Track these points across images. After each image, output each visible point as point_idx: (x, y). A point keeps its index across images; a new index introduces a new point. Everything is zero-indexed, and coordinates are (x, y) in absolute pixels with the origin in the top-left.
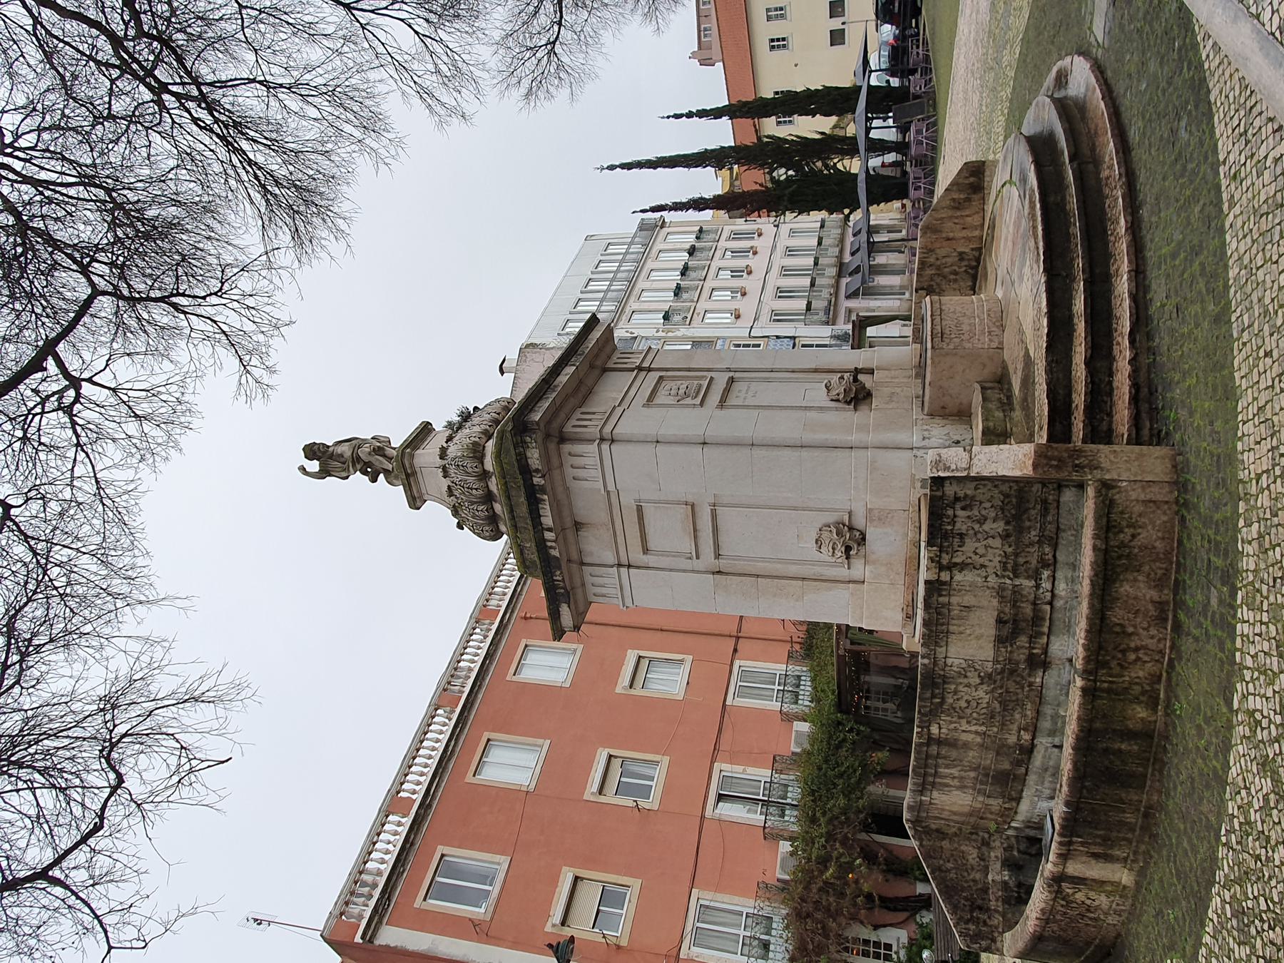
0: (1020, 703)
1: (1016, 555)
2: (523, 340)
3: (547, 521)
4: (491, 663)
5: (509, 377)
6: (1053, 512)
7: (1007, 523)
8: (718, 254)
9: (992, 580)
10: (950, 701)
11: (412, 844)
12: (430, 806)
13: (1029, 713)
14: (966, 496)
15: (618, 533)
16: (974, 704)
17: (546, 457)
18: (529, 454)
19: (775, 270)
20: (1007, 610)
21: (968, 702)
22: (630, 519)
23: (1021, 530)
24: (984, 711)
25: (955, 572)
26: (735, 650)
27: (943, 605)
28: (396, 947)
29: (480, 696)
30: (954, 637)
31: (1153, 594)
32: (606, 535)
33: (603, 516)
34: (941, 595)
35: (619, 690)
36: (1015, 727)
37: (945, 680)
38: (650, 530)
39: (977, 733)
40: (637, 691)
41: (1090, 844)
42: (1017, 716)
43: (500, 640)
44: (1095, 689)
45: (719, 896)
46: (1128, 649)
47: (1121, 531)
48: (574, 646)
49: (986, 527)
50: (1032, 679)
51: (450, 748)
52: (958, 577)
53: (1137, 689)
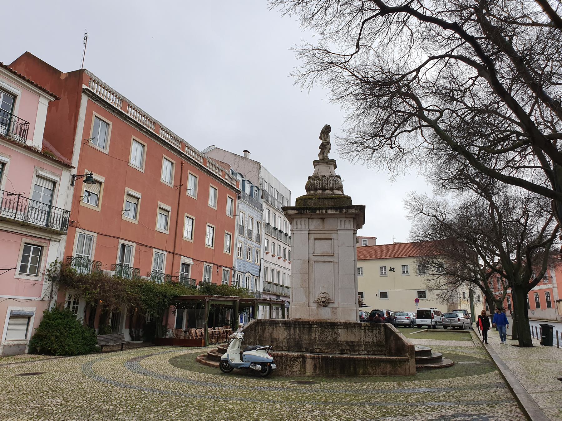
0: (328, 348)
1: (370, 345)
2: (262, 164)
3: (329, 211)
4: (169, 148)
5: (242, 154)
6: (380, 353)
7: (376, 343)
8: (285, 245)
9: (362, 340)
10: (326, 330)
11: (114, 111)
12: (125, 119)
13: (326, 350)
14: (381, 332)
15: (321, 231)
16: (326, 336)
17: (352, 214)
18: (353, 209)
19: (279, 269)
20: (356, 343)
21: (326, 335)
22: (327, 236)
23: (375, 346)
24: (324, 339)
25: (364, 330)
26: (170, 252)
27: (355, 327)
28: (81, 103)
29: (158, 143)
30: (346, 330)
31: (388, 372)
32: (320, 227)
33: (327, 227)
34: (358, 327)
35: (127, 188)
36: (320, 347)
37: (333, 329)
38: (322, 241)
39: (315, 337)
40: (158, 210)
41: (319, 364)
42: (324, 348)
43: (176, 152)
44: (365, 361)
45: (95, 245)
46: (376, 367)
47: (400, 364)
48: (173, 184)
49: (375, 338)
50: (337, 351)
51: (143, 129)
52: (363, 331)
53: (366, 370)
